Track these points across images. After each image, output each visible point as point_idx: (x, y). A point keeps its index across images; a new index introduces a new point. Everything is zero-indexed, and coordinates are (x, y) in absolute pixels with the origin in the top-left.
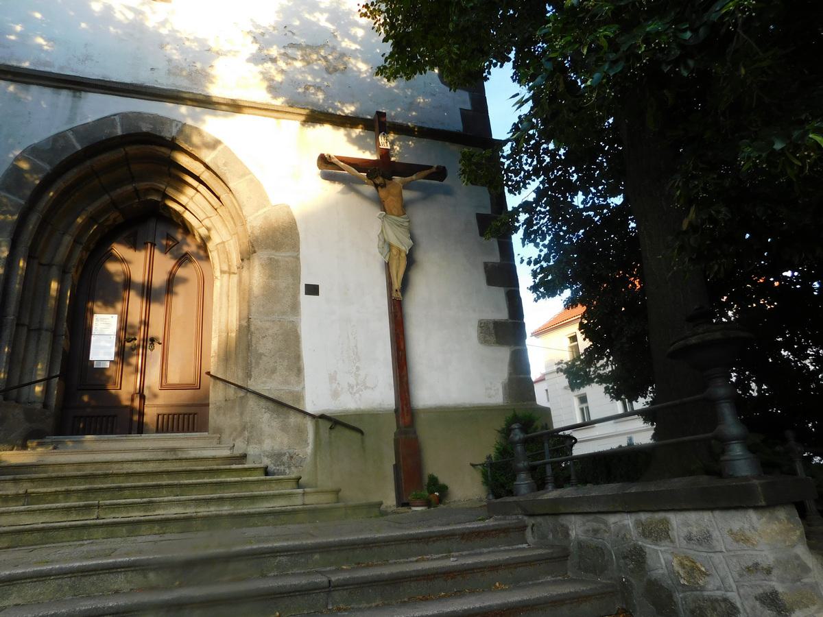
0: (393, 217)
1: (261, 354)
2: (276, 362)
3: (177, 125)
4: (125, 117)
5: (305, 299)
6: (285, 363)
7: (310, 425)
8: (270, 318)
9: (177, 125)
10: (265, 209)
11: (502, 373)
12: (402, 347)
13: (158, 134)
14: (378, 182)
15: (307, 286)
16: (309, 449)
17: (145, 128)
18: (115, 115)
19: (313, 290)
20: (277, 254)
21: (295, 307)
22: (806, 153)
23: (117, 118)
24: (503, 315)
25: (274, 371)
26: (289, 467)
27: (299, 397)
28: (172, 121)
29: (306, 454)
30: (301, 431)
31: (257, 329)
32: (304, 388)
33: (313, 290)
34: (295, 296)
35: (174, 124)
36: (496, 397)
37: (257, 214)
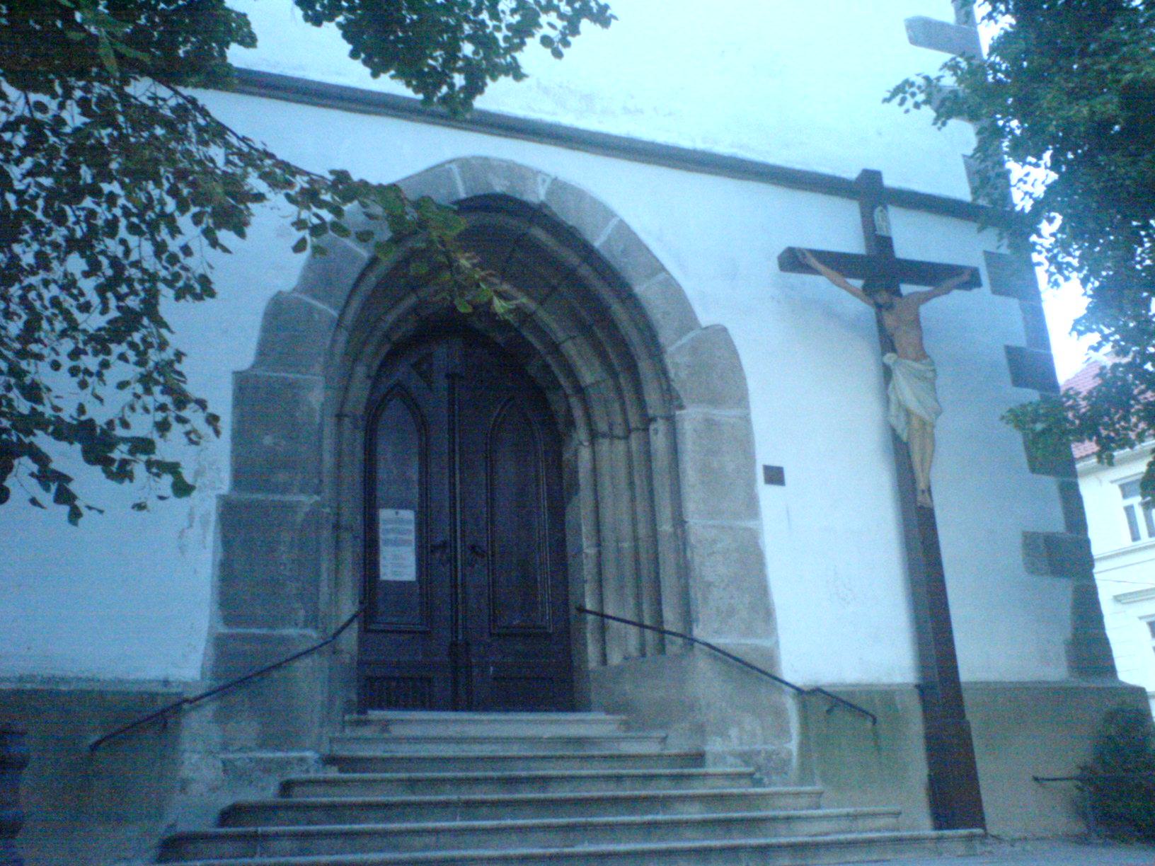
0: (908, 362)
1: (710, 584)
2: (732, 597)
3: (544, 181)
4: (465, 164)
5: (767, 494)
6: (306, 186)
7: (791, 705)
8: (717, 522)
9: (544, 181)
10: (691, 335)
11: (1061, 633)
12: (247, 88)
13: (518, 196)
14: (880, 301)
15: (768, 469)
16: (793, 746)
17: (499, 186)
18: (450, 162)
19: (775, 476)
20: (715, 412)
21: (752, 506)
22: (1010, 101)
23: (454, 167)
24: (1055, 522)
25: (731, 612)
26: (768, 774)
27: (771, 656)
28: (538, 173)
29: (789, 753)
30: (779, 713)
31: (700, 542)
32: (777, 643)
33: (775, 476)
34: (751, 484)
35: (539, 179)
36: (1056, 670)
37: (679, 343)
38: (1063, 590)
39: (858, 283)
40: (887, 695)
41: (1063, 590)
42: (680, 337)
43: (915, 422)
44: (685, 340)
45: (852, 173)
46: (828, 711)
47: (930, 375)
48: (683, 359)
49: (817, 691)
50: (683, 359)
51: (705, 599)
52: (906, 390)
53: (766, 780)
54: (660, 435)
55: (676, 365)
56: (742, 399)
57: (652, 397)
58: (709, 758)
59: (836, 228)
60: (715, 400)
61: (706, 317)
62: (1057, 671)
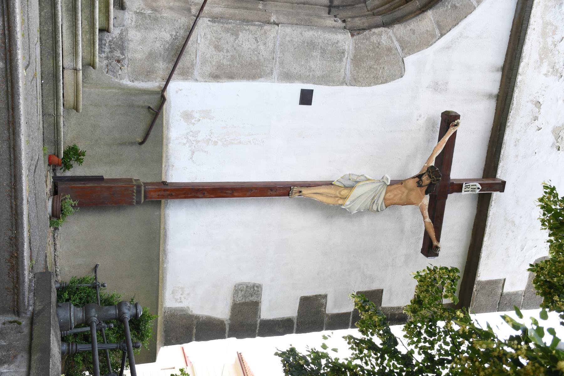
2: (228, 51)
7: (154, 85)
10: (399, 50)
14: (424, 178)
16: (126, 82)
19: (306, 98)
21: (288, 77)
26: (107, 58)
30: (148, 74)
31: (265, 33)
34: (300, 78)
38: (221, 311)
39: (433, 164)
40: (158, 158)
41: (221, 311)
42: (398, 40)
43: (345, 192)
44: (397, 44)
45: (501, 175)
46: (149, 108)
47: (375, 208)
48: (384, 39)
49: (163, 99)
50: (384, 39)
51: (227, 30)
52: (360, 196)
53: (103, 55)
54: (335, 23)
55: (380, 34)
56: (355, 81)
57: (358, 22)
58: (120, 13)
59: (465, 164)
60: (357, 61)
61: (410, 60)
62: (171, 300)
